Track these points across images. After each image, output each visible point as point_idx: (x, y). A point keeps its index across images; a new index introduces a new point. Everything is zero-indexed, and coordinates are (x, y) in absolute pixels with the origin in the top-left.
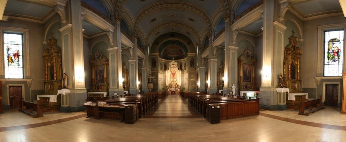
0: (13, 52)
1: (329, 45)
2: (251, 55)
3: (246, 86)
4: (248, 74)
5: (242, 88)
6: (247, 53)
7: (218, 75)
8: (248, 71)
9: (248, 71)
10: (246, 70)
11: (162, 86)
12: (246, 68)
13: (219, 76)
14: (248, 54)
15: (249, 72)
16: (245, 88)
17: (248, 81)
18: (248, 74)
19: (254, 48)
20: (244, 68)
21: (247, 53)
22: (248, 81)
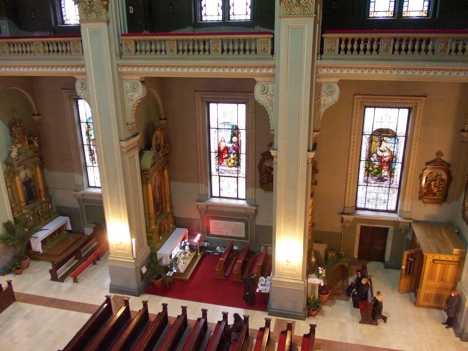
11: (282, 271)
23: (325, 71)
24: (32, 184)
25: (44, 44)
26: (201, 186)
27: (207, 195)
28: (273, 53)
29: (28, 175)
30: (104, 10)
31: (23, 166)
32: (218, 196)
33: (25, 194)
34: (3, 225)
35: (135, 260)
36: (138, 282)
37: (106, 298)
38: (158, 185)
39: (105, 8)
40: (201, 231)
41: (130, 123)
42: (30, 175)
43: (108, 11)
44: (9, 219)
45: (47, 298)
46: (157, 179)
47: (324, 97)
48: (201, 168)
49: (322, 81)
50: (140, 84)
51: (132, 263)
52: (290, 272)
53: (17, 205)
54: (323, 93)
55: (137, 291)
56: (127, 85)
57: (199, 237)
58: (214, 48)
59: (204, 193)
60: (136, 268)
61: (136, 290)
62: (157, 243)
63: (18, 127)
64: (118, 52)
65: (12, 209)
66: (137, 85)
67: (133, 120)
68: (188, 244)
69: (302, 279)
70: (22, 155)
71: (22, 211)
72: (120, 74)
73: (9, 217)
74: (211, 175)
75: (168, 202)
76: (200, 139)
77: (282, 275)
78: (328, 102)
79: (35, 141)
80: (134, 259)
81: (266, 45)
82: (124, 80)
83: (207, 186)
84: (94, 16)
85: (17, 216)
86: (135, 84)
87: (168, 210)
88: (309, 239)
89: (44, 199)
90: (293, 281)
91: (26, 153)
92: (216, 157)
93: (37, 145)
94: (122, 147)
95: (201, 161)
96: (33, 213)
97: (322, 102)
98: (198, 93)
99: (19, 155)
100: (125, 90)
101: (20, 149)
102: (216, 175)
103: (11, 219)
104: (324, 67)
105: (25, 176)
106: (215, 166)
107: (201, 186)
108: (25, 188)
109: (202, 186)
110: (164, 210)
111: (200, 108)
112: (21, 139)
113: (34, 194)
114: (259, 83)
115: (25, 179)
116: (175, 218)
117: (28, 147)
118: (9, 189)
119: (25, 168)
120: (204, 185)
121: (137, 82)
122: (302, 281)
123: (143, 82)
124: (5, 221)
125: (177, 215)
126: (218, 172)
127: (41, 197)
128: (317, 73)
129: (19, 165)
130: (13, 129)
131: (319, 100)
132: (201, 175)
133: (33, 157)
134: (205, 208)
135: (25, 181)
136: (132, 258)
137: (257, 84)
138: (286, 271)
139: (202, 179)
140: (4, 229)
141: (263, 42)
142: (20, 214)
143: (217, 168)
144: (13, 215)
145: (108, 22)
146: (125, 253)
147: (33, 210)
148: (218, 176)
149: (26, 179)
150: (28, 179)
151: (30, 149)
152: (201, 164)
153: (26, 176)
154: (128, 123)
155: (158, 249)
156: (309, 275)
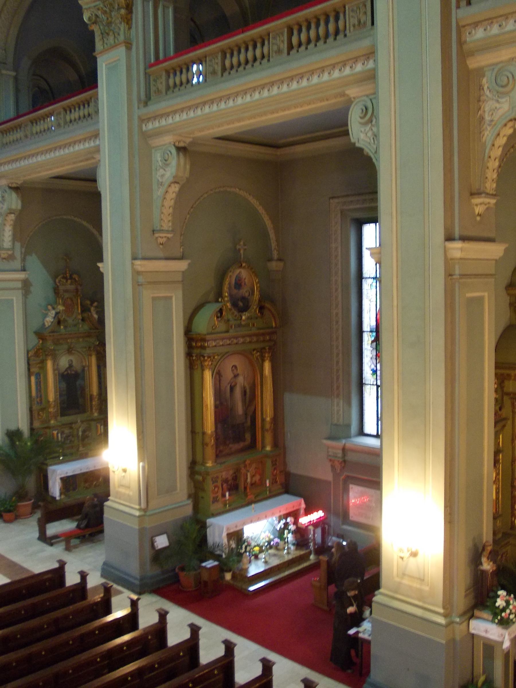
0: (406, 555)
1: (481, 204)
2: (256, 295)
3: (235, 478)
4: (240, 409)
5: (215, 500)
6: (238, 284)
7: (34, 370)
8: (238, 392)
9: (238, 392)
10: (232, 389)
11: (397, 579)
12: (228, 375)
13: (38, 375)
14: (244, 292)
15: (244, 393)
16: (222, 556)
17: (242, 445)
18: (240, 409)
19: (265, 235)
20: (218, 376)
21: (238, 284)
22: (242, 445)
23: (479, 33)
24: (79, 382)
25: (65, 110)
26: (335, 403)
27: (349, 426)
28: (373, 24)
29: (74, 364)
30: (123, 27)
31: (66, 347)
32: (375, 433)
33: (61, 395)
34: (6, 432)
35: (142, 513)
36: (142, 565)
37: (56, 565)
38: (244, 387)
39: (124, 22)
40: (332, 511)
41: (158, 228)
42: (77, 366)
43: (130, 28)
44: (20, 426)
45: (8, 559)
46: (239, 371)
47: (490, 103)
48: (338, 362)
49: (483, 64)
50: (174, 151)
51: (135, 516)
52: (416, 585)
53: (43, 409)
54: (488, 93)
55: (137, 582)
56: (158, 157)
57: (318, 517)
58: (275, 48)
59: (341, 420)
60: (142, 531)
61: (136, 579)
62: (213, 502)
63: (67, 280)
64: (143, 96)
65: (31, 411)
66: (170, 154)
67: (167, 225)
68: (292, 527)
69: (441, 611)
70: (65, 327)
71: (49, 421)
72: (146, 136)
73: (20, 422)
74: (361, 384)
75: (267, 430)
76: (337, 297)
77: (396, 592)
78: (500, 112)
79: (92, 309)
80: (140, 510)
81: (361, 10)
82: (154, 147)
83: (349, 404)
84: (111, 38)
85: (37, 424)
86: (169, 153)
87: (268, 448)
88: (493, 513)
89: (96, 414)
90: (419, 612)
91: (75, 325)
92: (372, 342)
93: (96, 316)
94: (137, 273)
95: (337, 347)
96: (70, 432)
97: (487, 118)
98: (336, 200)
99: (59, 323)
100: (153, 168)
101: (60, 315)
102: (372, 383)
103: (23, 425)
104: (476, 24)
105: (67, 366)
106: (370, 364)
107: (335, 403)
108: (64, 385)
109: (338, 405)
110: (259, 445)
111: (339, 232)
112: (69, 302)
113: (81, 401)
114: (357, 100)
115: (66, 370)
116: (288, 475)
117: (80, 317)
118: (33, 379)
119: (70, 351)
120: (341, 402)
121: (170, 149)
122: (445, 616)
123: (179, 149)
124: (13, 428)
125: (293, 469)
126: (375, 376)
127: (92, 409)
128: (461, 43)
129: (57, 342)
130: (57, 280)
131: (480, 112)
132: (338, 379)
133: (89, 336)
134: (340, 453)
135: (66, 373)
136: (137, 507)
137: (354, 103)
138: (406, 581)
139: (338, 388)
140: (6, 439)
141: (355, 8)
142: (46, 425)
143: (373, 367)
144: (31, 423)
145: (128, 45)
146: (129, 495)
147: (70, 425)
148: (375, 387)
149: (69, 372)
150: (73, 372)
151: (83, 320)
152: (338, 355)
153: (71, 366)
154: (155, 229)
155: (214, 515)
156: (477, 613)
